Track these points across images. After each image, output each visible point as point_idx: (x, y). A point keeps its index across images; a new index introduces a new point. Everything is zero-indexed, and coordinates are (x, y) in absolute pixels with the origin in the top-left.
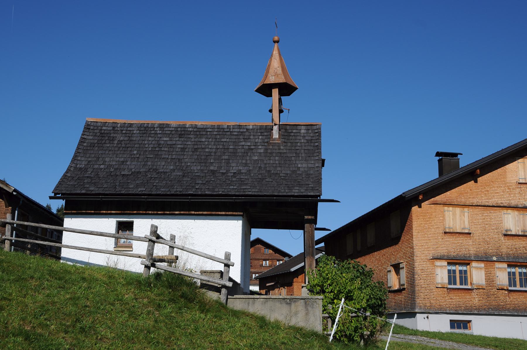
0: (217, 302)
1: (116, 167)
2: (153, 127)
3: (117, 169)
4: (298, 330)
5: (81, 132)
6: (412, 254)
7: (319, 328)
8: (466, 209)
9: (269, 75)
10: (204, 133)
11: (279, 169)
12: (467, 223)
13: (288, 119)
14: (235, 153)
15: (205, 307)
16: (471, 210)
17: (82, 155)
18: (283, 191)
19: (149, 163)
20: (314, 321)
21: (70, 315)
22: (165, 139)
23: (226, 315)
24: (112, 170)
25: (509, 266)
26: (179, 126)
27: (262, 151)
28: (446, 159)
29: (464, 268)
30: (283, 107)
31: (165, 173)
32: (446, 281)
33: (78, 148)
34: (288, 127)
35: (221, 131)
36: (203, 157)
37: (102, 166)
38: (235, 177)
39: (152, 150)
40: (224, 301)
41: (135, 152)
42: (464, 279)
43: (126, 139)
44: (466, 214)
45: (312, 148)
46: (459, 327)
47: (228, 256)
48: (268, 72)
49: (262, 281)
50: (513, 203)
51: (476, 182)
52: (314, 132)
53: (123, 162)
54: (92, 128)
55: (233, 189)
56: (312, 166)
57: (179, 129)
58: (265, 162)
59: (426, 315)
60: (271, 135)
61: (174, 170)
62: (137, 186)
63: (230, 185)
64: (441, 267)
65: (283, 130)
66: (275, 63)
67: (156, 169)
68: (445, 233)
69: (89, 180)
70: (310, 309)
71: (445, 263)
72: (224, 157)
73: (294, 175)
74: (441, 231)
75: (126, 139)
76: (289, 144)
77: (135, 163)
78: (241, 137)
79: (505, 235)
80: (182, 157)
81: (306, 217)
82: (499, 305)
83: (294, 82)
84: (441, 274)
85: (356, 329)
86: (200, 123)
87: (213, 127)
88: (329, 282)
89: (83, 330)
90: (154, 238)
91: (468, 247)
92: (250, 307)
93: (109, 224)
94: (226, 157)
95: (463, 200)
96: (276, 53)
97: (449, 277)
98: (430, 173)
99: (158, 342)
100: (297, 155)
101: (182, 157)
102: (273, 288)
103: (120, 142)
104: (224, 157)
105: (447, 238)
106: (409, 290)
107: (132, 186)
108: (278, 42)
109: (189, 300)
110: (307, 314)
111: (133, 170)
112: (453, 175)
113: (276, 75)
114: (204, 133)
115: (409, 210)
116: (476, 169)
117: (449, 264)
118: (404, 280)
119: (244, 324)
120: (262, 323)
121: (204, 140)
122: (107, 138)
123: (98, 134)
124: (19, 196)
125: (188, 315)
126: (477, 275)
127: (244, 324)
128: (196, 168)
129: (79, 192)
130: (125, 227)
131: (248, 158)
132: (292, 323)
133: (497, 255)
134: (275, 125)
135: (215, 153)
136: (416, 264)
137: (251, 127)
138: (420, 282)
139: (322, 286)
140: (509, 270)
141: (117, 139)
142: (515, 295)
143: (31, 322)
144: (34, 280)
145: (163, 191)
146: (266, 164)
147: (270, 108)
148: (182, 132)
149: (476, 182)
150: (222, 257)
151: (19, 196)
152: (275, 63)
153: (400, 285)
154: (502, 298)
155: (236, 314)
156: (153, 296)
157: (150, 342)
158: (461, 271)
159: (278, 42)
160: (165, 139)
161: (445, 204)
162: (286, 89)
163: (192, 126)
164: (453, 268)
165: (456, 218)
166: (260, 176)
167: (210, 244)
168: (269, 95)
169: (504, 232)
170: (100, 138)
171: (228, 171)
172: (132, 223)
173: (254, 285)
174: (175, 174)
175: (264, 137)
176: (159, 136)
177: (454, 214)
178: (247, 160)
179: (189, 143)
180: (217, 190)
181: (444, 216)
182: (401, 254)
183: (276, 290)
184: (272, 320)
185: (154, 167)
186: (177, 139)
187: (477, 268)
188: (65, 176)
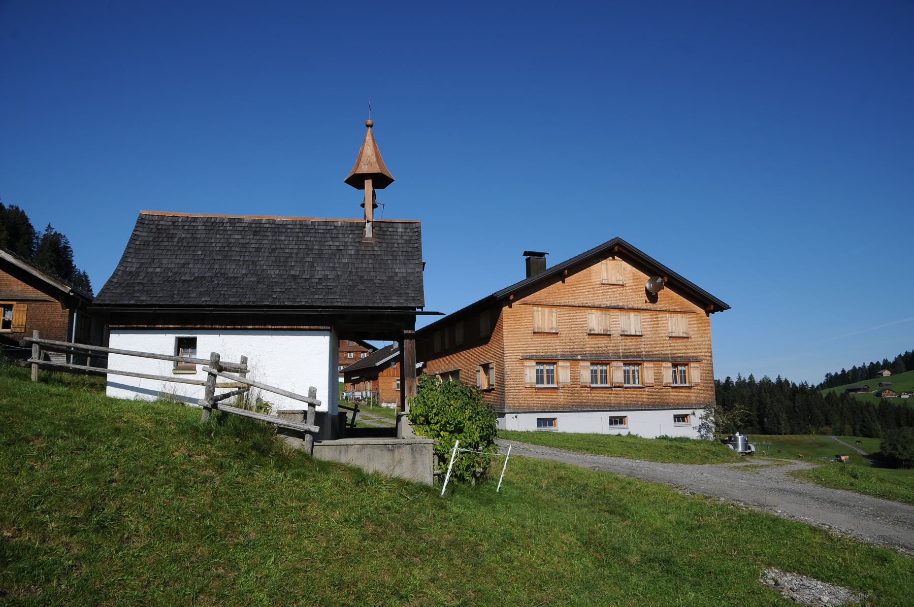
0: (299, 452)
1: (176, 270)
2: (222, 222)
3: (176, 273)
4: (403, 484)
5: (133, 227)
6: (503, 354)
7: (429, 480)
8: (554, 310)
9: (361, 164)
10: (284, 230)
11: (373, 274)
12: (554, 323)
13: (383, 215)
14: (320, 254)
15: (283, 461)
16: (559, 309)
17: (132, 255)
18: (379, 302)
19: (216, 266)
20: (423, 470)
21: (81, 500)
22: (236, 237)
23: (311, 471)
24: (170, 274)
25: (592, 364)
26: (254, 222)
27: (353, 252)
28: (534, 259)
29: (551, 367)
30: (377, 201)
31: (235, 278)
32: (535, 381)
33: (128, 247)
34: (383, 225)
35: (304, 227)
36: (282, 259)
37: (158, 270)
38: (321, 284)
39: (220, 251)
40: (309, 451)
41: (199, 253)
42: (551, 378)
43: (188, 236)
44: (554, 314)
45: (411, 250)
46: (545, 425)
47: (313, 393)
48: (360, 160)
49: (348, 375)
50: (597, 303)
51: (564, 282)
52: (413, 231)
53: (184, 264)
54: (146, 222)
55: (318, 299)
56: (412, 271)
57: (254, 225)
58: (357, 265)
59: (514, 415)
60: (363, 233)
61: (246, 275)
62: (201, 295)
63: (314, 293)
64: (530, 367)
65: (377, 228)
66: (369, 150)
67: (225, 274)
68: (535, 333)
69: (141, 287)
70: (417, 456)
71: (533, 363)
72: (307, 260)
73: (391, 282)
74: (531, 331)
75: (188, 236)
76: (385, 245)
77: (199, 266)
78: (328, 235)
79: (589, 334)
80: (256, 259)
81: (405, 332)
82: (582, 402)
83: (390, 173)
84: (530, 374)
85: (467, 468)
86: (279, 218)
87: (294, 223)
88: (435, 411)
89: (101, 528)
90: (215, 371)
91: (555, 346)
92: (342, 456)
93: (165, 342)
94: (310, 260)
95: (551, 301)
96: (369, 138)
97: (537, 377)
98: (518, 275)
99: (215, 535)
100: (394, 258)
101: (256, 259)
102: (358, 381)
103: (181, 240)
104: (307, 260)
105: (538, 339)
106: (498, 389)
107: (193, 295)
108: (371, 126)
109: (263, 452)
110: (414, 463)
111: (196, 275)
112: (540, 276)
113: (370, 164)
114: (284, 230)
115: (500, 311)
116: (564, 269)
117: (537, 363)
118: (493, 381)
119: (336, 483)
120: (359, 477)
121: (283, 238)
122: (164, 235)
123: (154, 230)
124: (77, 297)
125: (260, 476)
126: (563, 373)
127: (336, 483)
128: (273, 272)
129: (126, 302)
130: (187, 344)
131: (336, 260)
132: (395, 475)
133: (581, 354)
134: (368, 222)
135: (297, 254)
136: (506, 365)
137: (340, 224)
138: (509, 382)
139: (426, 417)
140: (592, 368)
141: (178, 236)
142: (596, 392)
143: (14, 522)
144: (41, 439)
145: (232, 301)
146: (357, 268)
147: (362, 202)
148: (257, 228)
149: (564, 282)
150: (306, 394)
151: (77, 297)
152: (369, 150)
153: (489, 385)
154: (585, 395)
155: (325, 467)
156: (213, 451)
157: (203, 536)
158: (548, 370)
159: (371, 126)
160: (236, 237)
161: (534, 305)
162: (381, 181)
163: (269, 222)
164: (541, 367)
165: (544, 319)
166: (351, 283)
167: (291, 369)
168: (361, 187)
169: (588, 332)
170: (157, 235)
171: (312, 276)
172: (195, 339)
173: (341, 376)
174: (247, 279)
175: (355, 236)
176: (229, 233)
177: (543, 315)
178: (334, 263)
179: (266, 242)
180: (298, 300)
181: (533, 317)
182: (491, 354)
183: (361, 384)
184: (371, 472)
185: (223, 271)
186: (251, 237)
187: (563, 367)
188: (110, 281)
